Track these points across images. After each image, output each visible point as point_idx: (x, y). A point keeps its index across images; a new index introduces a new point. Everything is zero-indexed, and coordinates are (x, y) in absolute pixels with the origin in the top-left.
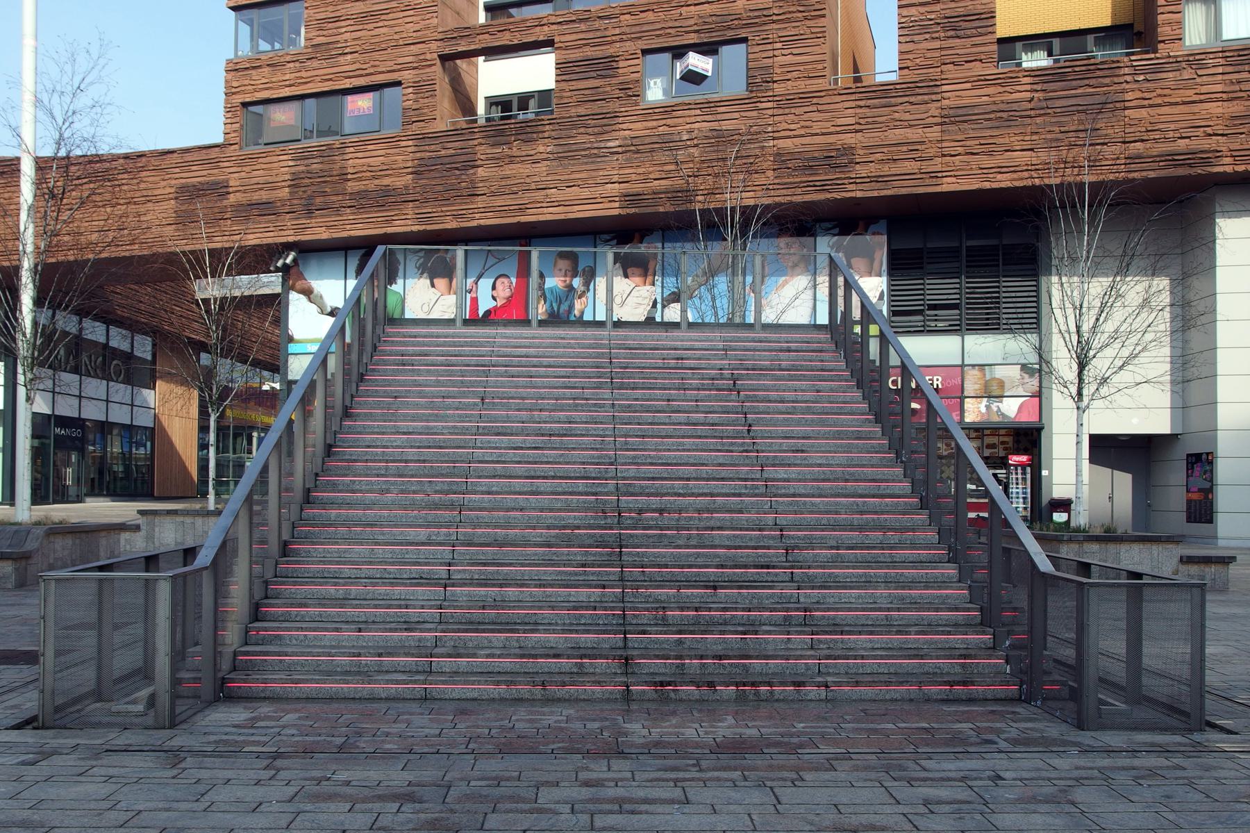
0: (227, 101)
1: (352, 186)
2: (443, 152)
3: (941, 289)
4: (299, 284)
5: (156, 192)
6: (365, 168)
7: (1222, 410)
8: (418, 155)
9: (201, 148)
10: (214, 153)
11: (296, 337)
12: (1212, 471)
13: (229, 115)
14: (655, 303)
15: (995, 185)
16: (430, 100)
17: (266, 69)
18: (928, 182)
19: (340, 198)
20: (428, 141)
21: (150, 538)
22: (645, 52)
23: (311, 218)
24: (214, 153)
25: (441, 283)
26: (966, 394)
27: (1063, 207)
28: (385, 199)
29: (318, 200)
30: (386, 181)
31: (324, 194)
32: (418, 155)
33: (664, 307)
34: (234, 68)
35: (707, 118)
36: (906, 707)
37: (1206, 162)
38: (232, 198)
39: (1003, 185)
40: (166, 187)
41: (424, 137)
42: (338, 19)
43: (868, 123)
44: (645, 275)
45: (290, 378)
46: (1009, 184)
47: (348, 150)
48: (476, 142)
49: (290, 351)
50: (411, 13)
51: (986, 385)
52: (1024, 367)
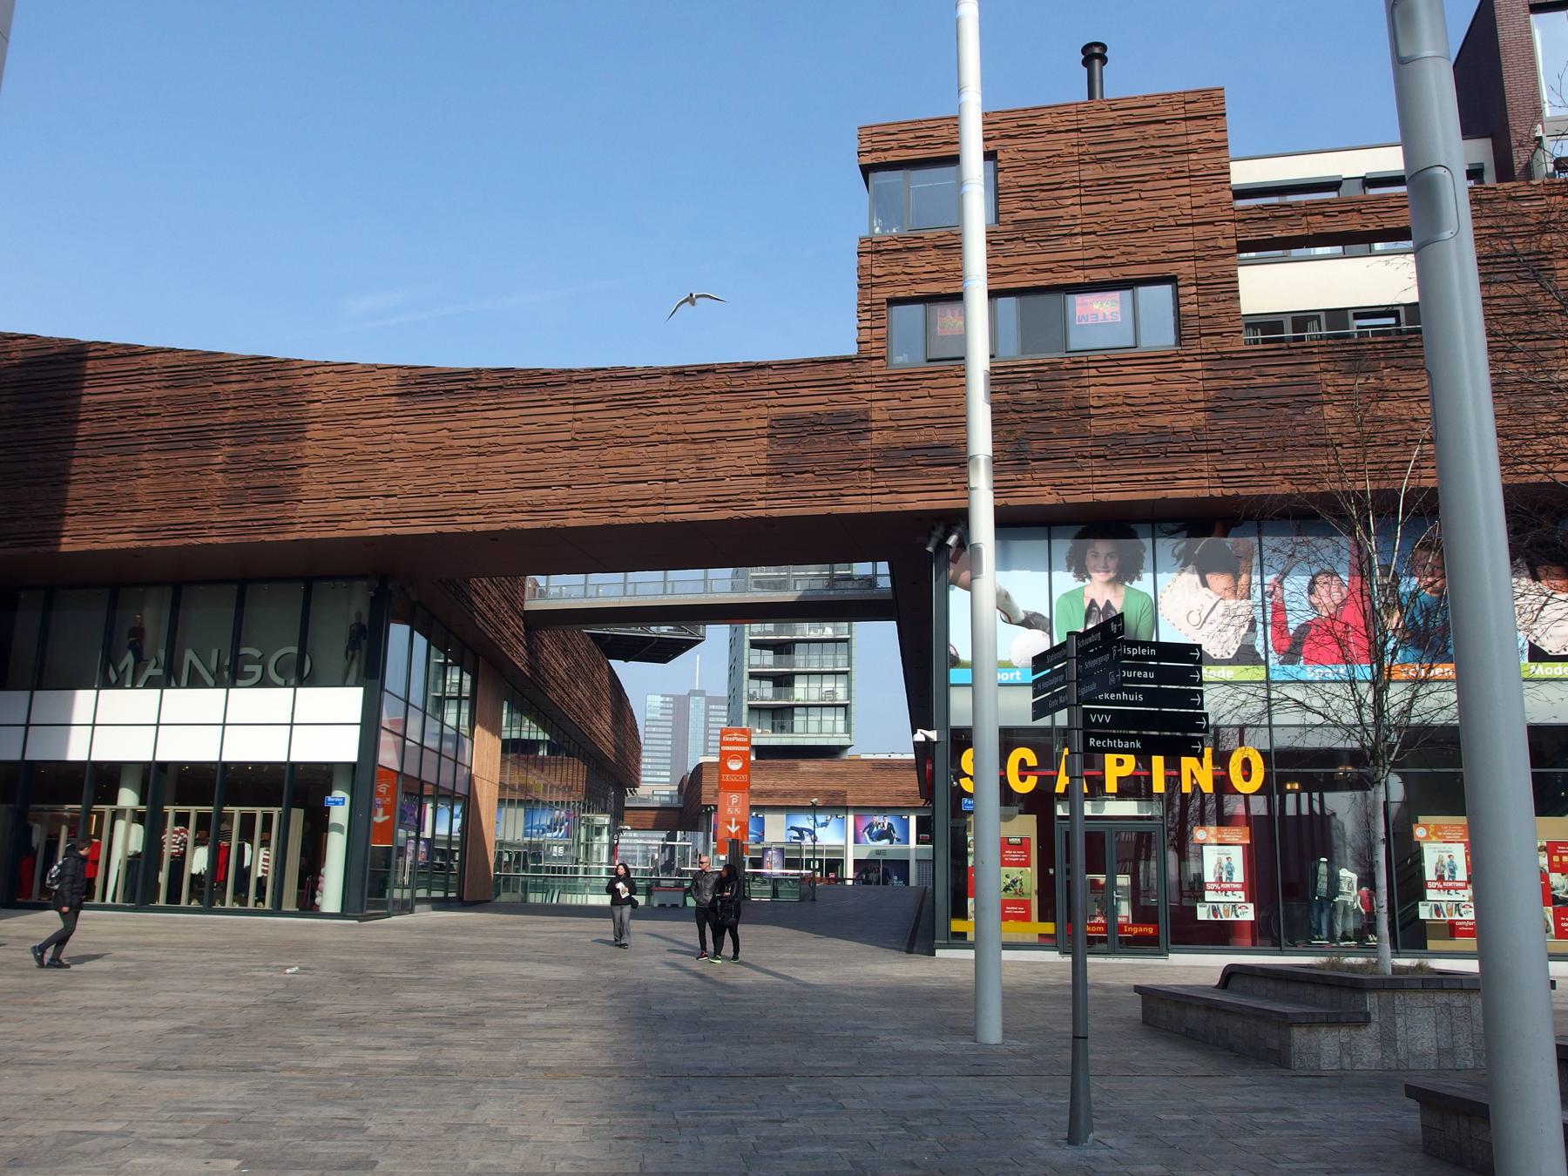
0: (862, 296)
1: (1097, 426)
2: (1259, 381)
5: (733, 426)
6: (1119, 400)
8: (1215, 383)
9: (815, 362)
10: (840, 371)
13: (867, 316)
14: (1253, 623)
15: (624, 521)
17: (934, 252)
19: (1077, 443)
21: (1387, 1040)
22: (893, 302)
24: (840, 371)
25: (1219, 581)
28: (1162, 447)
29: (1036, 445)
30: (1160, 420)
31: (1047, 436)
32: (1215, 383)
34: (872, 249)
35: (782, 401)
37: (746, 503)
38: (876, 438)
39: (632, 520)
40: (756, 416)
41: (1224, 357)
42: (1058, 186)
43: (585, 439)
46: (639, 520)
47: (1085, 373)
48: (1316, 368)
50: (1186, 181)
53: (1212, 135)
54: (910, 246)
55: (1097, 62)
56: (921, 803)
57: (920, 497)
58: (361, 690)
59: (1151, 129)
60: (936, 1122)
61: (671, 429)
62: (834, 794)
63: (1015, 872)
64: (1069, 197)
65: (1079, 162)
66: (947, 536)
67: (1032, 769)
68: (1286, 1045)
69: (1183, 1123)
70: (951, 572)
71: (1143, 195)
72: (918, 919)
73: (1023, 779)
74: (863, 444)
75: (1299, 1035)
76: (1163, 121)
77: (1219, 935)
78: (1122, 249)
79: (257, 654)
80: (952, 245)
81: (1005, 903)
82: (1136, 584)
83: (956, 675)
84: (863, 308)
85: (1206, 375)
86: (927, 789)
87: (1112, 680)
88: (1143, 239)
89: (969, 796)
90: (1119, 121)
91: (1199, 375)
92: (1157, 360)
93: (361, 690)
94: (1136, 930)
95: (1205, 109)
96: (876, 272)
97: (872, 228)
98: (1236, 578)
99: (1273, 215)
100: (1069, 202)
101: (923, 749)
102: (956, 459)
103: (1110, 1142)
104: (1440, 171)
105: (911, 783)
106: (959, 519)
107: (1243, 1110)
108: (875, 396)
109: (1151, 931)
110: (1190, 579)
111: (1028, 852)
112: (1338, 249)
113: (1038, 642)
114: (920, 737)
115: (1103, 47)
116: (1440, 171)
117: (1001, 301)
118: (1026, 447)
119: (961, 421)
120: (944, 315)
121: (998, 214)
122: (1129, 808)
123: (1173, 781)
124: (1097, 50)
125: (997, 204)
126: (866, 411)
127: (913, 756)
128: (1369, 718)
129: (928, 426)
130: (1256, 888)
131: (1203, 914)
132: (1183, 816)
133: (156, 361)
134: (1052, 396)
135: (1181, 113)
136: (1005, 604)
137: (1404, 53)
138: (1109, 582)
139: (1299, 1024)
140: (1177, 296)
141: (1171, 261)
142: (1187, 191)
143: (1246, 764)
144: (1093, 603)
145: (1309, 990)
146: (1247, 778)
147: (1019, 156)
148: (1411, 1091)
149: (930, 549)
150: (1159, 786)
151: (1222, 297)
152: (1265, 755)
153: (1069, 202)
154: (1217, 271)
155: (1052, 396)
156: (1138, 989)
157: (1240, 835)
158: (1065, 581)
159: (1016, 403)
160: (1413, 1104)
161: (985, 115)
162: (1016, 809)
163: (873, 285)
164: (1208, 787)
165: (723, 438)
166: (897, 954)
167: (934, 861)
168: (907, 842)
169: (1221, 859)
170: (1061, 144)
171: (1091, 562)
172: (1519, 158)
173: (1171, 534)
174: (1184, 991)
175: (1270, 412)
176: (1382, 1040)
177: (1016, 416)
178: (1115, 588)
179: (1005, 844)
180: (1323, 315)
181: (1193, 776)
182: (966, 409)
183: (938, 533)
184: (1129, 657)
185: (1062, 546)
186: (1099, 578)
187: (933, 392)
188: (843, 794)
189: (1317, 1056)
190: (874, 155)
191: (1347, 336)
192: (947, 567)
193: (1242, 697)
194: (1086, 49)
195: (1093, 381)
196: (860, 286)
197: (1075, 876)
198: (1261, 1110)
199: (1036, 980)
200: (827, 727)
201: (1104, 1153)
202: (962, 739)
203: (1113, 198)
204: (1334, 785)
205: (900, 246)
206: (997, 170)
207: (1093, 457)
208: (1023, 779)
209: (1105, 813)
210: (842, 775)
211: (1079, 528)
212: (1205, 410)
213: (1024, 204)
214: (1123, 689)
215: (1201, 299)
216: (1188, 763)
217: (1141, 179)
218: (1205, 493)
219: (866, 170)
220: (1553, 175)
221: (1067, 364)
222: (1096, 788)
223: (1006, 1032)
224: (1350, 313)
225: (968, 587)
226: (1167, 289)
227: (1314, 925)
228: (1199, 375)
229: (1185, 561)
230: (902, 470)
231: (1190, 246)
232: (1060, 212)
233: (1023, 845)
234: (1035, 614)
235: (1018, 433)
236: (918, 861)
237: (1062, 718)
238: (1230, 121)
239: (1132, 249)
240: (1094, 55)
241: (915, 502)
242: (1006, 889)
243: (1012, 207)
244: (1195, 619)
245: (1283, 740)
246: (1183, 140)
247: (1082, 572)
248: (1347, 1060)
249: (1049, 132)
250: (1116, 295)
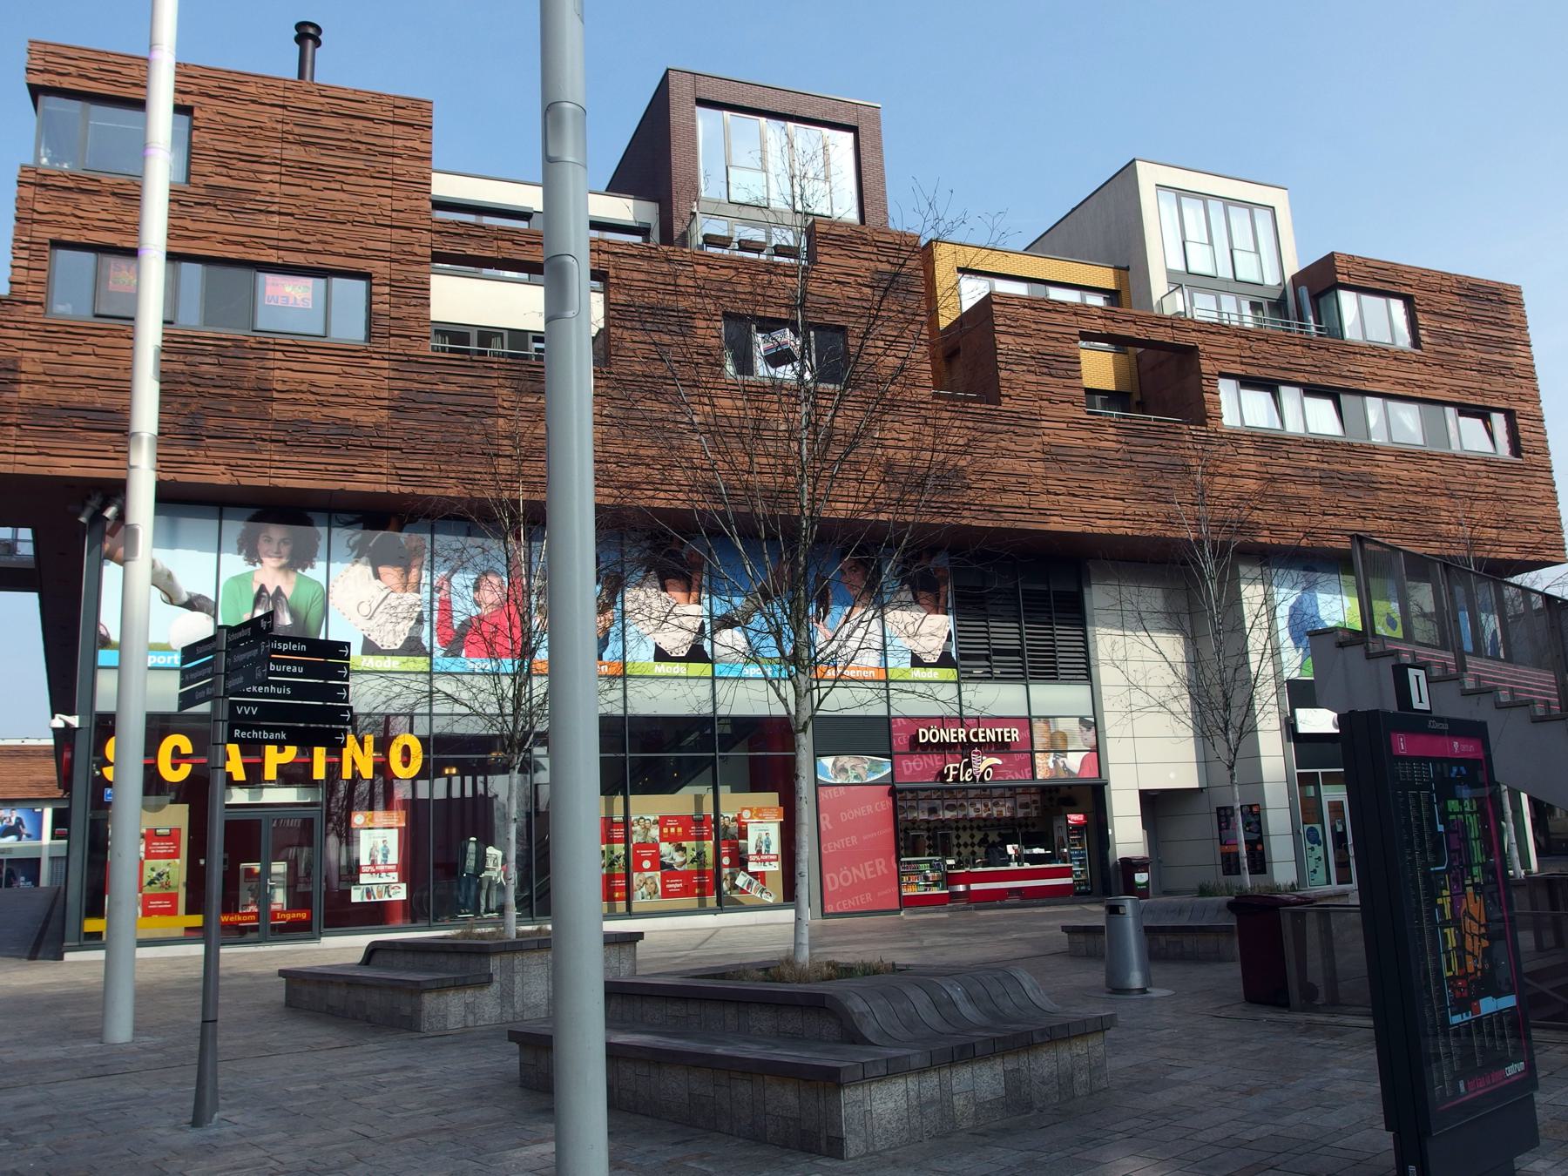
0: (19, 231)
1: (278, 410)
2: (442, 387)
3: (1005, 633)
6: (304, 387)
7: (1264, 761)
8: (400, 384)
12: (1259, 823)
13: (25, 254)
16: (418, 309)
17: (111, 199)
18: (1037, 518)
19: (256, 424)
20: (415, 367)
21: (506, 996)
22: (57, 244)
23: (197, 448)
25: (391, 574)
26: (1036, 748)
28: (343, 439)
29: (212, 422)
30: (344, 413)
32: (400, 384)
33: (713, 632)
34: (34, 181)
38: (25, 392)
41: (410, 360)
42: (258, 160)
44: (688, 590)
47: (271, 355)
50: (389, 183)
51: (1052, 738)
52: (1082, 720)
53: (417, 144)
54: (83, 187)
55: (310, 43)
56: (60, 793)
57: (71, 463)
58: (187, 806)
59: (358, 124)
60: (47, 1127)
63: (161, 864)
64: (269, 174)
65: (283, 140)
66: (104, 507)
67: (186, 757)
68: (417, 1011)
69: (310, 1092)
70: (107, 546)
71: (345, 187)
72: (46, 922)
73: (175, 767)
74: (8, 396)
75: (429, 1001)
76: (371, 120)
77: (375, 914)
78: (319, 237)
80: (131, 195)
81: (146, 899)
82: (309, 572)
83: (106, 657)
84: (19, 245)
85: (392, 374)
86: (66, 780)
87: (259, 675)
88: (341, 231)
89: (109, 784)
90: (326, 108)
91: (385, 373)
92: (346, 353)
93: (187, 806)
94: (289, 917)
95: (413, 118)
96: (39, 207)
97: (38, 157)
98: (407, 572)
99: (467, 232)
100: (268, 178)
101: (64, 736)
102: (118, 424)
103: (234, 1119)
104: (570, 259)
105: (47, 772)
106: (116, 490)
107: (370, 1073)
108: (27, 345)
109: (304, 916)
110: (363, 570)
111: (177, 843)
112: (525, 276)
113: (199, 627)
114: (59, 722)
115: (319, 30)
116: (570, 259)
117: (186, 267)
118: (201, 423)
119: (125, 386)
120: (117, 268)
121: (189, 174)
122: (289, 795)
123: (333, 769)
124: (311, 31)
125: (189, 163)
126: (15, 360)
127: (51, 742)
128: (508, 709)
129: (89, 386)
130: (410, 869)
131: (357, 896)
132: (340, 804)
134: (234, 373)
135: (389, 116)
136: (164, 583)
137: (551, 154)
138: (281, 568)
139: (430, 990)
140: (370, 294)
141: (367, 258)
142: (388, 192)
143: (406, 751)
144: (262, 588)
145: (443, 958)
146: (406, 763)
147: (218, 118)
148: (513, 1036)
149: (83, 519)
150: (319, 773)
151: (414, 302)
152: (424, 741)
153: (268, 178)
154: (411, 276)
155: (234, 373)
156: (282, 973)
157: (398, 818)
158: (234, 564)
159: (193, 375)
160: (515, 1047)
161: (178, 65)
162: (168, 798)
163: (35, 221)
164: (368, 773)
166: (15, 962)
167: (67, 858)
168: (39, 837)
169: (378, 841)
170: (266, 116)
171: (263, 546)
172: (678, 228)
173: (347, 525)
174: (328, 971)
175: (451, 418)
176: (502, 997)
177: (193, 389)
178: (286, 575)
179: (151, 836)
180: (506, 334)
181: (354, 763)
182: (132, 374)
183: (94, 504)
184: (280, 652)
185: (235, 528)
186: (271, 563)
187: (99, 351)
189: (445, 1017)
190: (47, 76)
191: (526, 357)
192: (102, 540)
193: (397, 689)
194: (301, 26)
195: (279, 364)
196: (18, 219)
197: (225, 868)
198: (384, 1071)
199: (179, 974)
201: (227, 1130)
202: (106, 726)
203: (315, 184)
204: (487, 769)
205: (71, 184)
206: (193, 128)
207: (272, 441)
208: (175, 767)
209: (262, 801)
211: (253, 511)
212: (389, 408)
213: (219, 170)
214: (273, 682)
215: (394, 300)
216: (351, 749)
217: (345, 171)
218: (382, 489)
219: (36, 91)
220: (701, 247)
221: (252, 343)
222: (254, 777)
223: (137, 1030)
224: (530, 336)
225: (122, 562)
226: (361, 285)
227: (461, 900)
228: (385, 373)
229: (359, 552)
230: (55, 431)
231: (387, 246)
232: (257, 186)
233: (173, 836)
234: (200, 597)
235: (193, 408)
236: (52, 859)
237: (205, 708)
238: (436, 134)
239: (330, 239)
240: (307, 34)
241: (68, 467)
242: (151, 883)
243: (207, 169)
244: (365, 610)
245: (441, 726)
246: (389, 142)
247: (253, 556)
248: (471, 1018)
249: (253, 102)
250: (309, 281)
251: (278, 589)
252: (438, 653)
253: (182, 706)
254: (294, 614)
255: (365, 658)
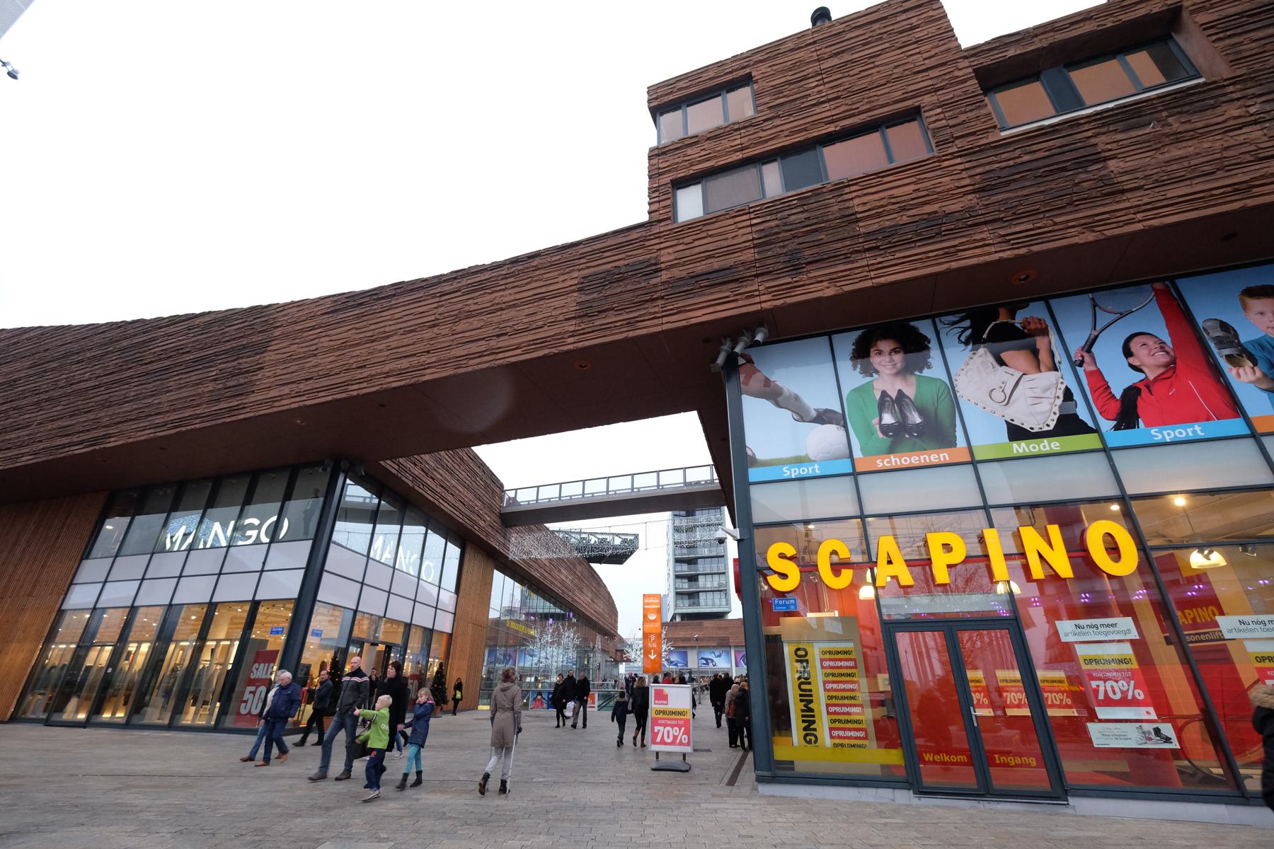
2: (1026, 158)
4: (755, 383)
11: (760, 456)
27: (167, 694)
36: (204, 526)
42: (805, 78)
45: (758, 518)
49: (751, 479)
61: (505, 299)
62: (722, 639)
65: (818, 60)
79: (256, 522)
133: (197, 321)
138: (898, 374)
144: (884, 394)
158: (852, 377)
159: (785, 225)
165: (543, 298)
178: (905, 379)
188: (728, 639)
200: (717, 601)
210: (726, 628)
212: (974, 192)
234: (827, 411)
244: (998, 396)
251: (900, 391)
252: (1106, 425)
253: (814, 24)
254: (921, 412)
255: (1015, 445)
